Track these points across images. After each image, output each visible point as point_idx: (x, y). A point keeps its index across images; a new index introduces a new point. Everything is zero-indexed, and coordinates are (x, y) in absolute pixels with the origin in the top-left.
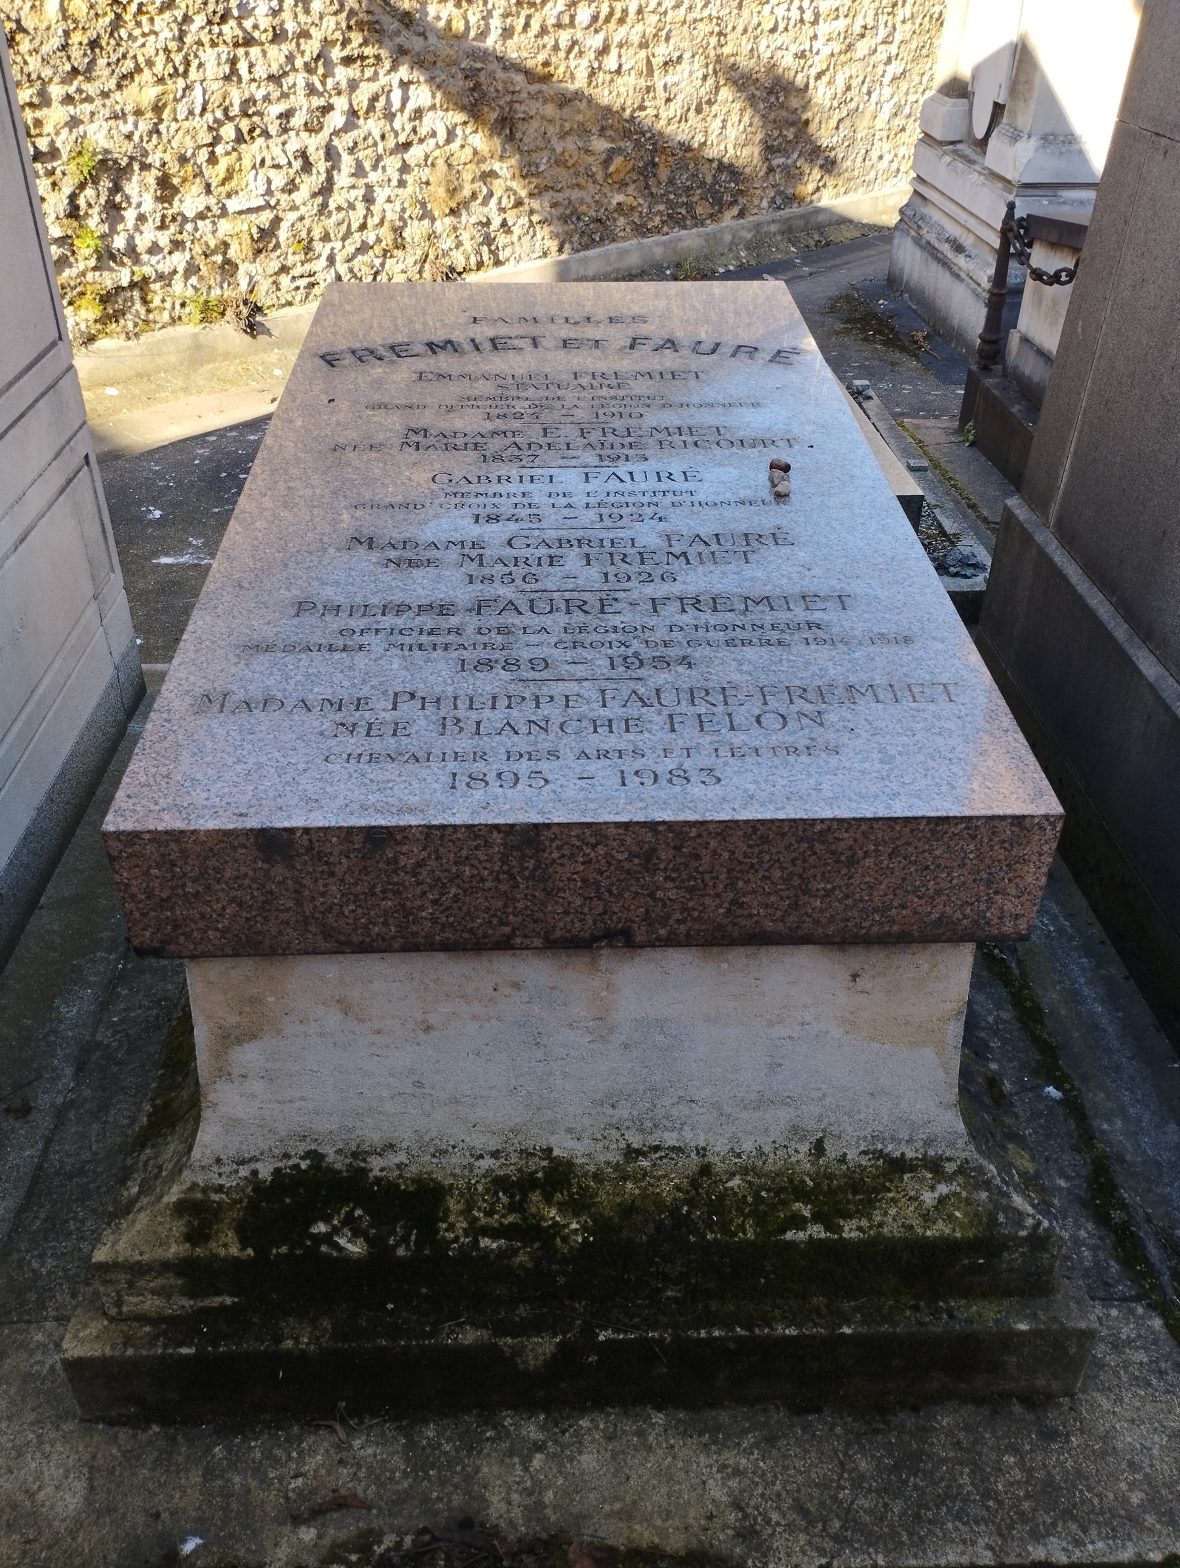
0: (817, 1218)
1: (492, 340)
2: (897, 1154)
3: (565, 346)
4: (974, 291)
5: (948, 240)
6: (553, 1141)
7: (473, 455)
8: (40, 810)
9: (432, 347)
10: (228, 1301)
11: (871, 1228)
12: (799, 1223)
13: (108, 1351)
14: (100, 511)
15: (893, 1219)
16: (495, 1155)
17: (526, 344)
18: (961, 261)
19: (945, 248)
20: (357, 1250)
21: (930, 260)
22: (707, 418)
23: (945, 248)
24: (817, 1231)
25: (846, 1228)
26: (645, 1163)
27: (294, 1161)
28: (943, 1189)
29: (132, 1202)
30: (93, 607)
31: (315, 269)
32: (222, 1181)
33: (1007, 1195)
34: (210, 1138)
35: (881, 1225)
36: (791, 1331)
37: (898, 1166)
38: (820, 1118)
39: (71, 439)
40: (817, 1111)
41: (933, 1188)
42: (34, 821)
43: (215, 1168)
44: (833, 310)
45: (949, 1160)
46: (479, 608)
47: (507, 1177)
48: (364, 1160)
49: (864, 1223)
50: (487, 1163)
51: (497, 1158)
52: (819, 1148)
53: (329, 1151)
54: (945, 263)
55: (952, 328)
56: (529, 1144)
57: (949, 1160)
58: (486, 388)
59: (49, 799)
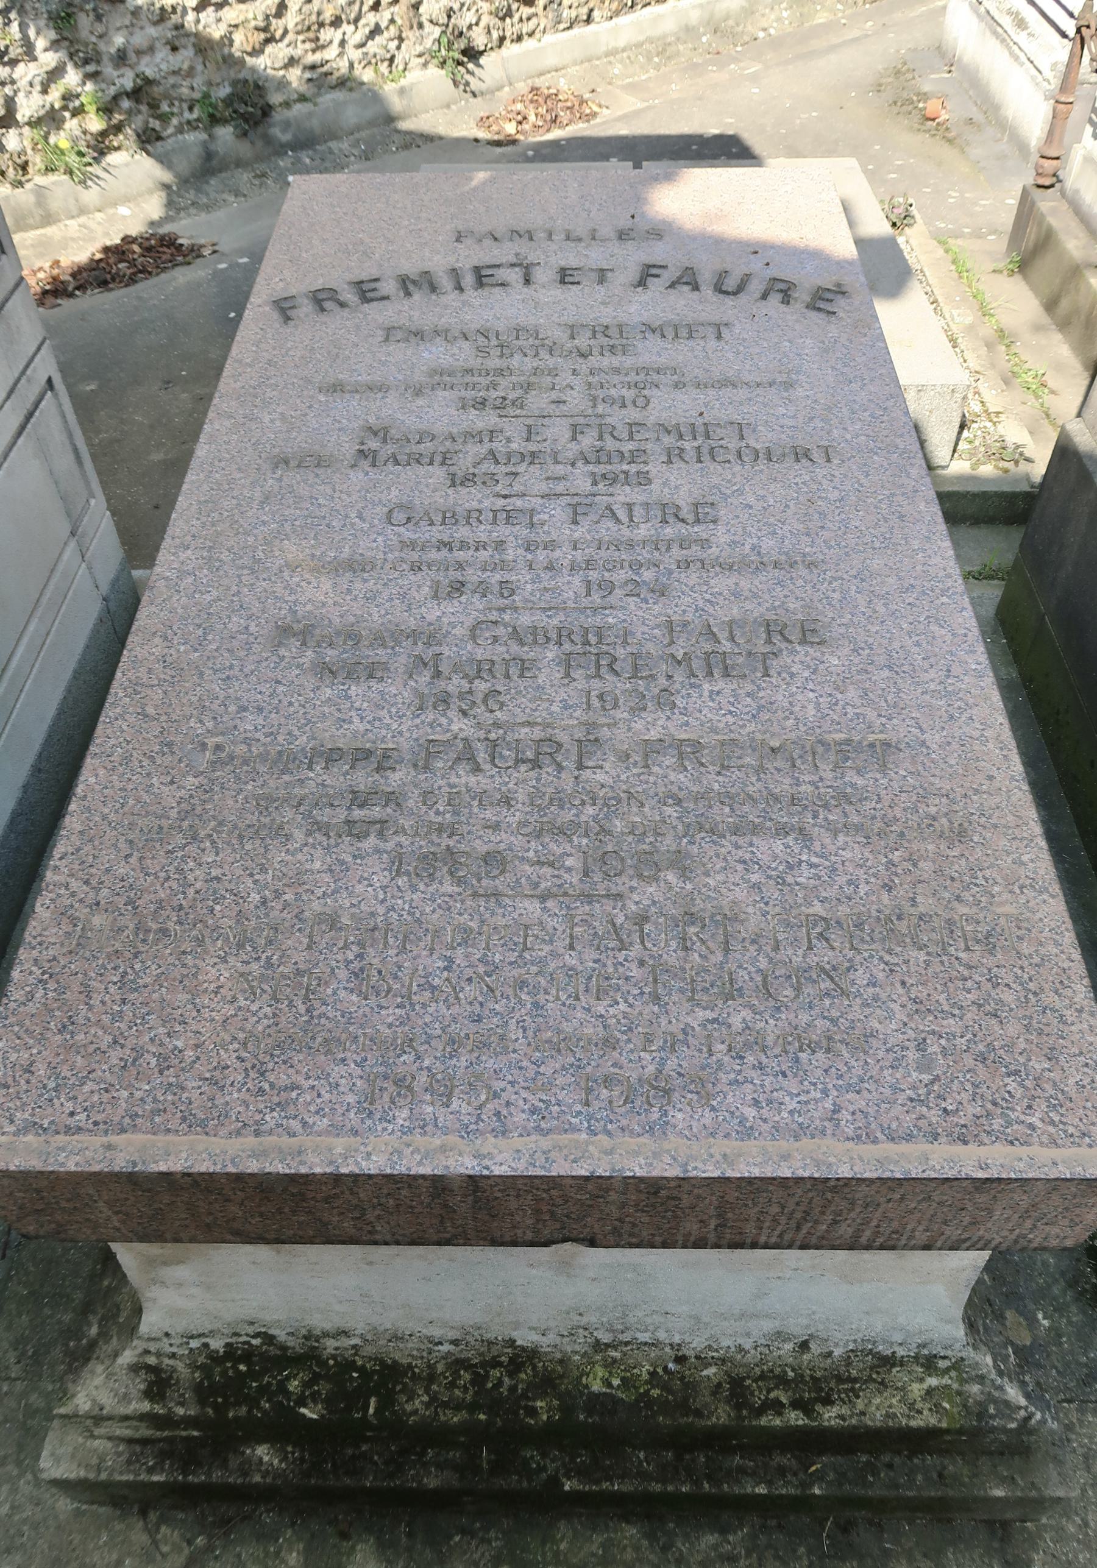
0: (796, 1405)
1: (477, 270)
2: (889, 1352)
3: (563, 282)
4: (1033, 78)
5: (1009, 12)
6: (515, 1335)
7: (438, 473)
8: (26, 787)
9: (406, 284)
10: (195, 1433)
11: (851, 1416)
12: (777, 1407)
13: (82, 1473)
14: (71, 436)
15: (877, 1409)
16: (455, 1342)
17: (514, 276)
18: (1021, 37)
19: (1006, 21)
20: (315, 1416)
21: (988, 33)
22: (720, 407)
23: (1006, 21)
24: (796, 1418)
25: (826, 1416)
26: (614, 1354)
27: (244, 1339)
28: (933, 1381)
29: (93, 1345)
30: (72, 544)
31: (327, 57)
32: (174, 1349)
33: (1001, 1388)
34: (151, 1322)
35: (863, 1413)
36: (762, 1490)
37: (888, 1362)
38: (808, 1327)
39: (27, 366)
40: (805, 1322)
41: (922, 1380)
42: (20, 802)
43: (165, 1340)
44: (878, 88)
45: (944, 1358)
46: (428, 753)
47: (469, 1359)
48: (317, 1341)
49: (845, 1410)
50: (445, 1348)
51: (457, 1345)
52: (804, 1346)
53: (281, 1335)
54: (1004, 39)
55: (1006, 118)
56: (490, 1336)
57: (944, 1358)
58: (463, 354)
59: (37, 769)
